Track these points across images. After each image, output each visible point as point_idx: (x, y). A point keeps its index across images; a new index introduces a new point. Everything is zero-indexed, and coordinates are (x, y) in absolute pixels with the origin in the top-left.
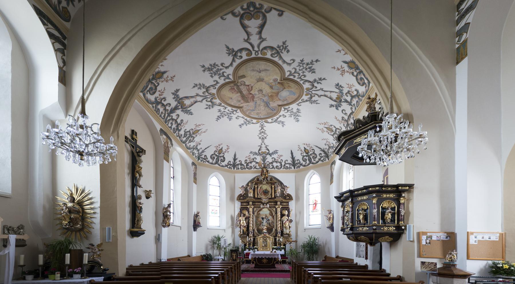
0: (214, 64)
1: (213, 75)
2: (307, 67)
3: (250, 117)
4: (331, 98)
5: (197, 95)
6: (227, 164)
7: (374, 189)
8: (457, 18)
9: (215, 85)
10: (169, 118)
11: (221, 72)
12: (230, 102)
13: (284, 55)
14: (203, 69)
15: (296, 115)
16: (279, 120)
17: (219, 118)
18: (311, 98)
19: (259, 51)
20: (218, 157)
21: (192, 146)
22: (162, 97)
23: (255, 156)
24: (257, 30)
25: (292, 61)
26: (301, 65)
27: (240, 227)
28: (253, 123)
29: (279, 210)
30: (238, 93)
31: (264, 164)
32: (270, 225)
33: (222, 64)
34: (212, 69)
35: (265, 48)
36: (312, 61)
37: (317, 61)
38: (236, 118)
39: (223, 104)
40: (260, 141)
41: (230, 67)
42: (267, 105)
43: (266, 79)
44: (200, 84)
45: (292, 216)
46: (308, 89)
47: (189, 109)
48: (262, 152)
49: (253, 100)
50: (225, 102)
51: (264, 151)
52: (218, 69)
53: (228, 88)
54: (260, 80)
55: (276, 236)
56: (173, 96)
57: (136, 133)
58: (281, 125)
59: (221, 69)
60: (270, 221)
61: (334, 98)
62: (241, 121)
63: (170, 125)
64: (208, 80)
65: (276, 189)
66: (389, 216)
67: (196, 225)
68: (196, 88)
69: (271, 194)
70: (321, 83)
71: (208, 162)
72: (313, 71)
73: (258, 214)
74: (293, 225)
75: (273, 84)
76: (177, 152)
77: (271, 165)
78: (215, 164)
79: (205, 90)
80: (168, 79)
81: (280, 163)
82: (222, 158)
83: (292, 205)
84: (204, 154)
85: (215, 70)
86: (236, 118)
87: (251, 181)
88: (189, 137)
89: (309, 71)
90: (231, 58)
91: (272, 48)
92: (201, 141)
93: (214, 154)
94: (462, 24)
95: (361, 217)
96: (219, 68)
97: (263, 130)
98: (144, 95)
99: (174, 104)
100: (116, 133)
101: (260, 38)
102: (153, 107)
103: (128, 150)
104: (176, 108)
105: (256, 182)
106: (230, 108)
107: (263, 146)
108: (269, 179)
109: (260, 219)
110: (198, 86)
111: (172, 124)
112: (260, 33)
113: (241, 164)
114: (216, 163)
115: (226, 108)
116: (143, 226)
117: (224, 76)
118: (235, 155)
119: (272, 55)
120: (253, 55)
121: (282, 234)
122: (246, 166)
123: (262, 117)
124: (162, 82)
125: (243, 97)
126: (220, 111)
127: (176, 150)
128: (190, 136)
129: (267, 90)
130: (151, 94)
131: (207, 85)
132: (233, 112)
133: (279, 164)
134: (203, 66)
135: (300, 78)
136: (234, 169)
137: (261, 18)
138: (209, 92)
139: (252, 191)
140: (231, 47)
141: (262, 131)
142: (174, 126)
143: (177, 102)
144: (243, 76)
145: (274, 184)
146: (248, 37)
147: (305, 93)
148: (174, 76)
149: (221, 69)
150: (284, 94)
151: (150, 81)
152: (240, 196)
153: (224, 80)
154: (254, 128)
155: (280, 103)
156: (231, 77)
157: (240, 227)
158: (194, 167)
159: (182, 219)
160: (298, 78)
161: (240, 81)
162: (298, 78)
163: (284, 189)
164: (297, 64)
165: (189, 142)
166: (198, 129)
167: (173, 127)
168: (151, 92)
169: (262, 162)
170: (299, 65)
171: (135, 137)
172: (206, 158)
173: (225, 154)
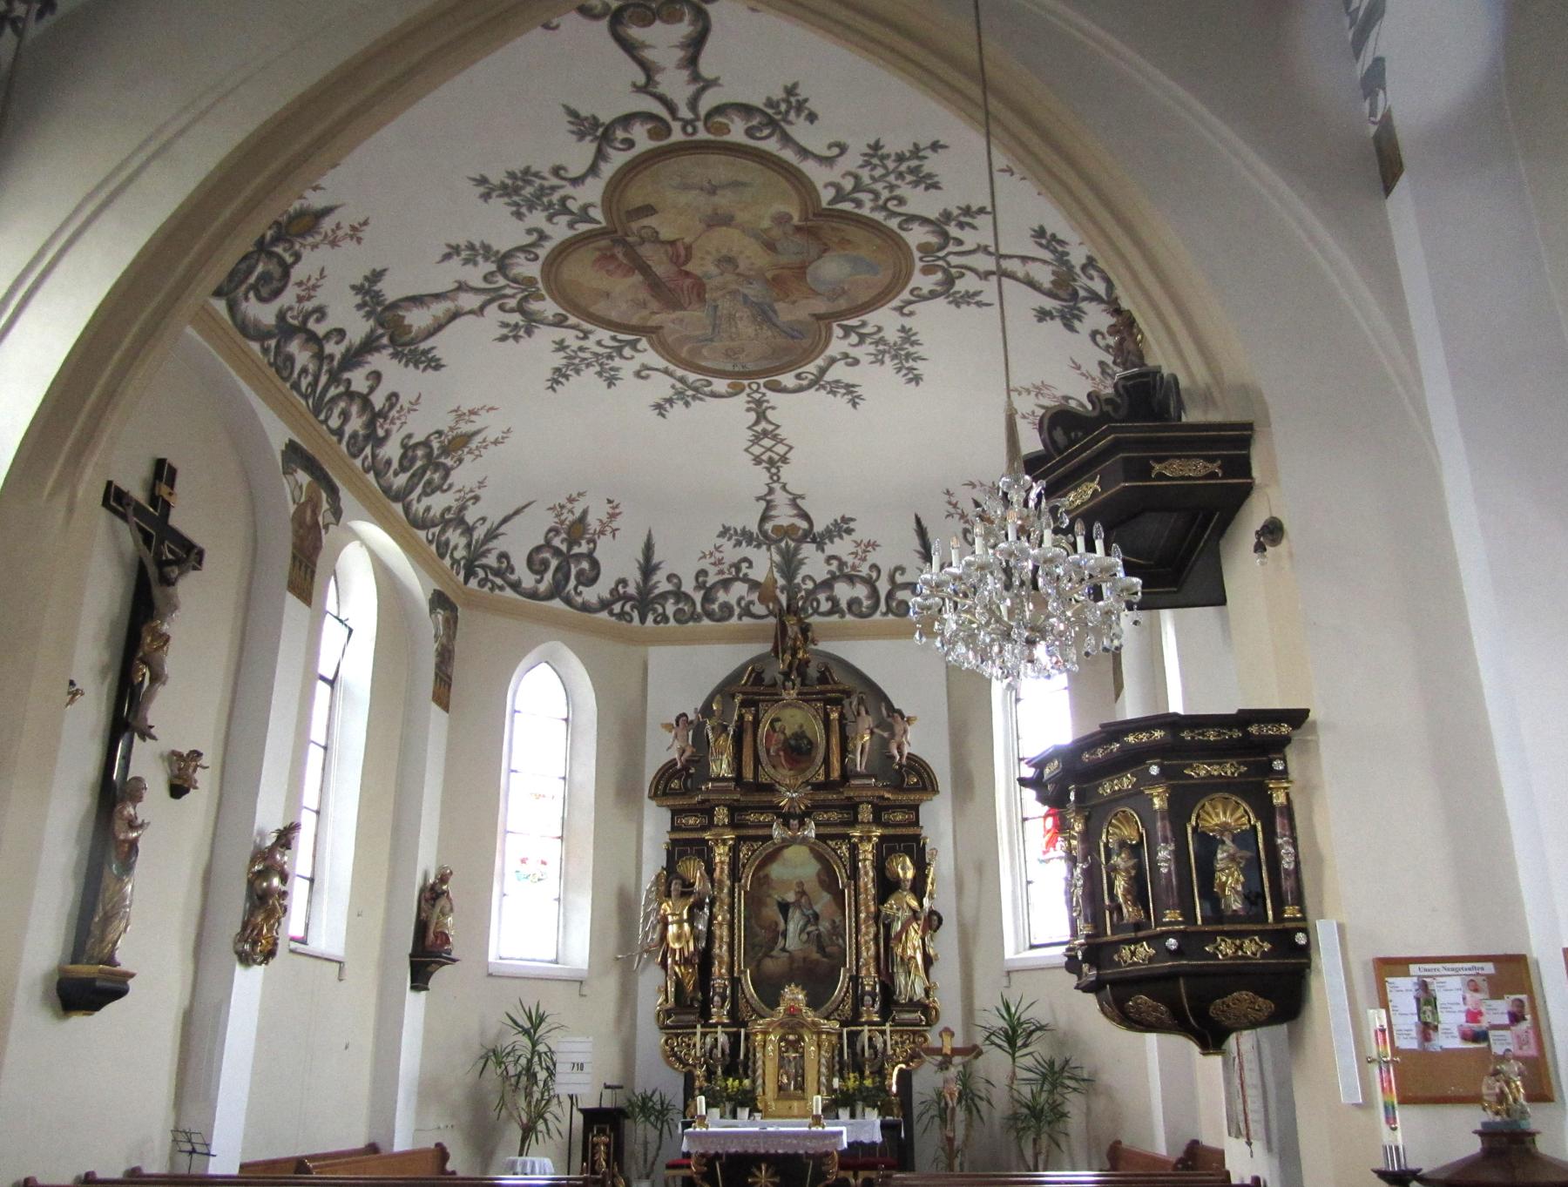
0: (527, 171)
1: (524, 210)
2: (903, 167)
3: (697, 366)
4: (1031, 284)
5: (462, 287)
6: (606, 595)
7: (1144, 737)
8: (1350, 36)
9: (533, 245)
10: (333, 392)
11: (555, 197)
12: (600, 308)
13: (799, 130)
14: (482, 190)
15: (903, 355)
16: (829, 377)
17: (558, 377)
18: (949, 281)
19: (697, 118)
20: (566, 559)
21: (436, 511)
22: (309, 306)
23: (747, 551)
24: (680, 54)
25: (836, 151)
26: (875, 161)
27: (664, 964)
28: (714, 395)
29: (867, 852)
30: (629, 272)
31: (791, 590)
32: (821, 949)
33: (556, 171)
34: (519, 189)
35: (720, 110)
36: (915, 145)
37: (935, 146)
38: (638, 374)
39: (573, 320)
40: (761, 476)
41: (589, 181)
42: (764, 315)
43: (742, 216)
44: (471, 247)
45: (940, 897)
46: (925, 249)
47: (423, 346)
48: (776, 529)
49: (701, 298)
50: (577, 306)
51: (784, 521)
52: (542, 188)
53: (587, 254)
54: (719, 220)
55: (855, 1019)
56: (358, 299)
57: (173, 472)
58: (841, 401)
59: (553, 188)
60: (824, 926)
61: (1047, 285)
62: (661, 386)
63: (334, 422)
64: (503, 228)
65: (849, 731)
66: (1230, 881)
67: (427, 956)
68: (456, 262)
69: (827, 761)
70: (974, 228)
71: (515, 586)
72: (930, 183)
73: (761, 881)
74: (946, 944)
75: (776, 233)
76: (364, 543)
77: (822, 597)
78: (550, 596)
79: (493, 267)
80: (340, 233)
81: (870, 583)
82: (585, 565)
83: (938, 821)
84: (498, 545)
85: (528, 191)
86: (638, 374)
87: (725, 690)
88: (424, 470)
89: (916, 184)
90: (588, 149)
91: (746, 110)
92: (481, 484)
93: (548, 544)
94: (1367, 59)
95: (1120, 885)
96: (546, 184)
97: (763, 425)
98: (232, 308)
99: (358, 328)
100: (63, 499)
101: (696, 77)
102: (265, 351)
103: (121, 555)
104: (369, 345)
105: (747, 691)
106: (604, 335)
107: (780, 498)
108: (813, 672)
109: (772, 912)
110: (464, 254)
111: (345, 416)
112: (692, 62)
113: (679, 595)
114: (556, 591)
115: (586, 336)
116: (126, 955)
117: (565, 210)
118: (649, 548)
119: (750, 132)
120: (677, 136)
121: (888, 999)
122: (700, 607)
123: (751, 367)
124: (314, 246)
125: (655, 285)
126: (561, 346)
127: (356, 536)
128: (432, 462)
129: (752, 255)
130: (261, 299)
131: (503, 246)
132: (619, 350)
133: (861, 591)
134: (483, 181)
135: (884, 208)
136: (643, 620)
137: (687, 18)
138: (515, 271)
139: (726, 743)
140: (584, 113)
141: (764, 430)
142: (356, 424)
143: (371, 322)
144: (648, 210)
145: (837, 702)
146: (649, 78)
147: (919, 265)
148: (365, 223)
149: (553, 188)
150: (831, 269)
151: (262, 247)
152: (668, 772)
153: (571, 225)
154: (724, 417)
155: (821, 306)
156: (596, 213)
157: (664, 964)
158: (440, 615)
159: (356, 913)
160: (873, 209)
161: (635, 226)
162: (873, 209)
163: (890, 728)
164: (860, 161)
165: (425, 493)
166: (465, 428)
167: (348, 430)
168: (264, 292)
169: (781, 582)
170: (867, 163)
171: (164, 490)
172: (504, 567)
173: (602, 542)
